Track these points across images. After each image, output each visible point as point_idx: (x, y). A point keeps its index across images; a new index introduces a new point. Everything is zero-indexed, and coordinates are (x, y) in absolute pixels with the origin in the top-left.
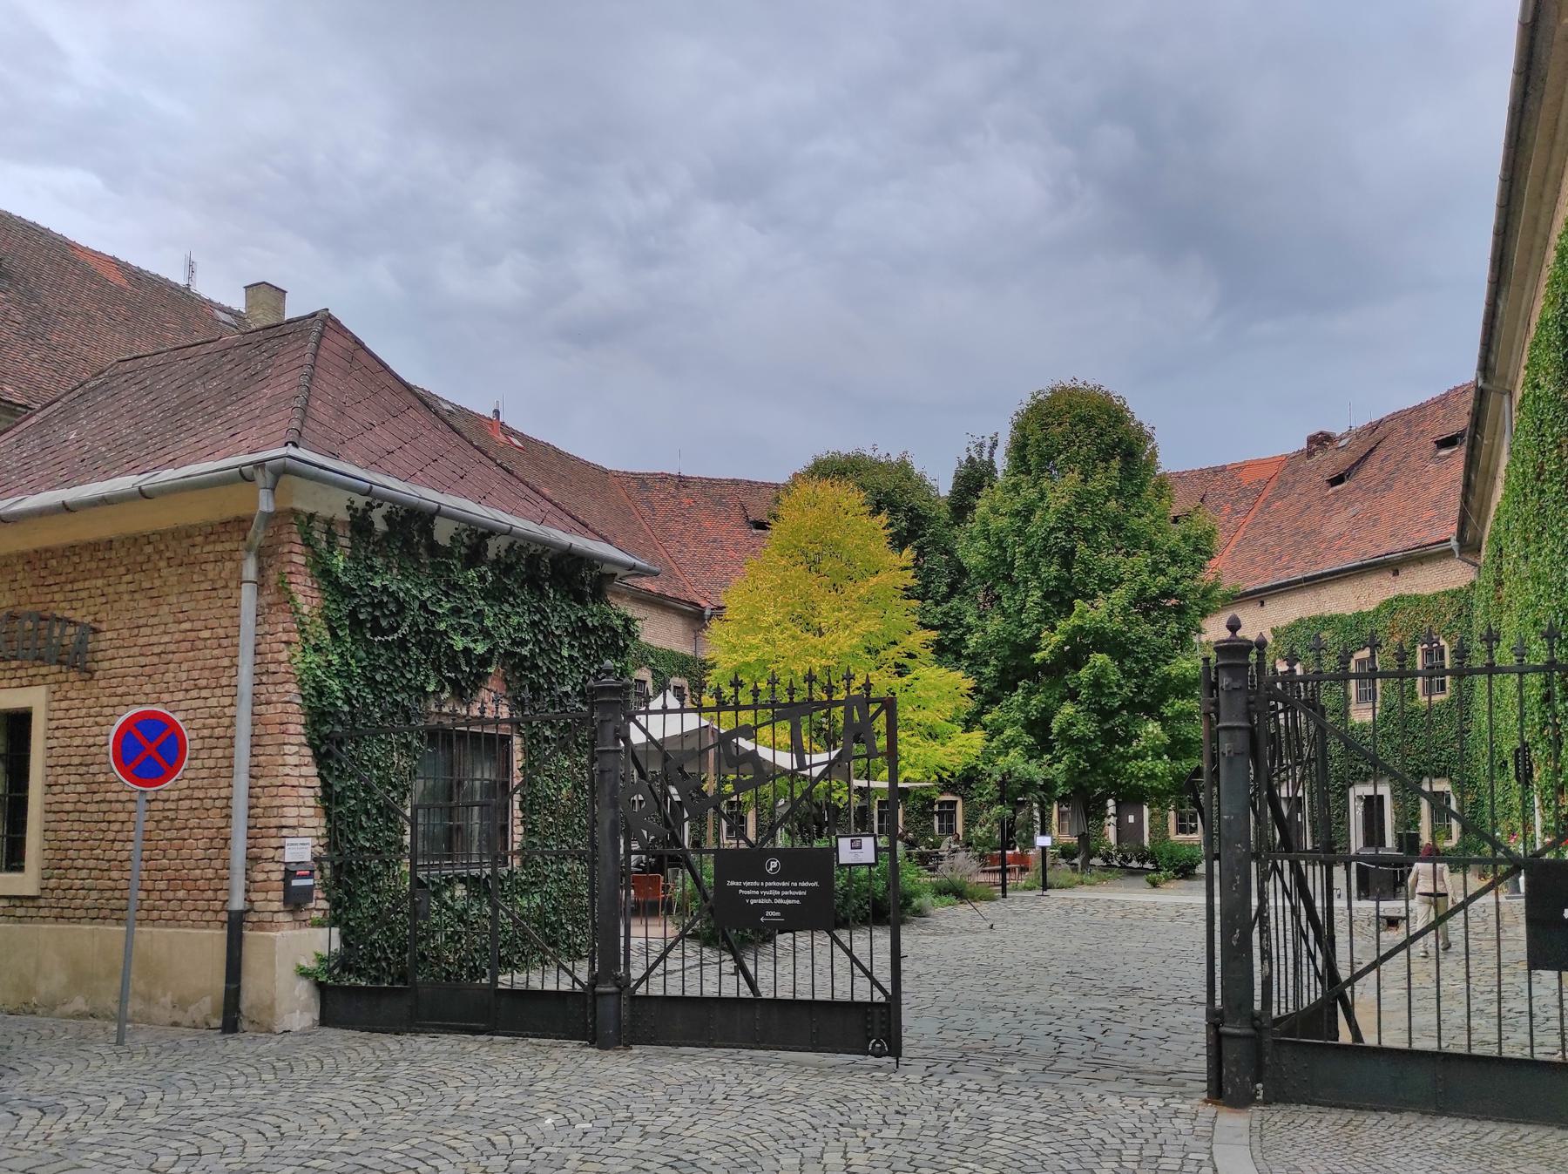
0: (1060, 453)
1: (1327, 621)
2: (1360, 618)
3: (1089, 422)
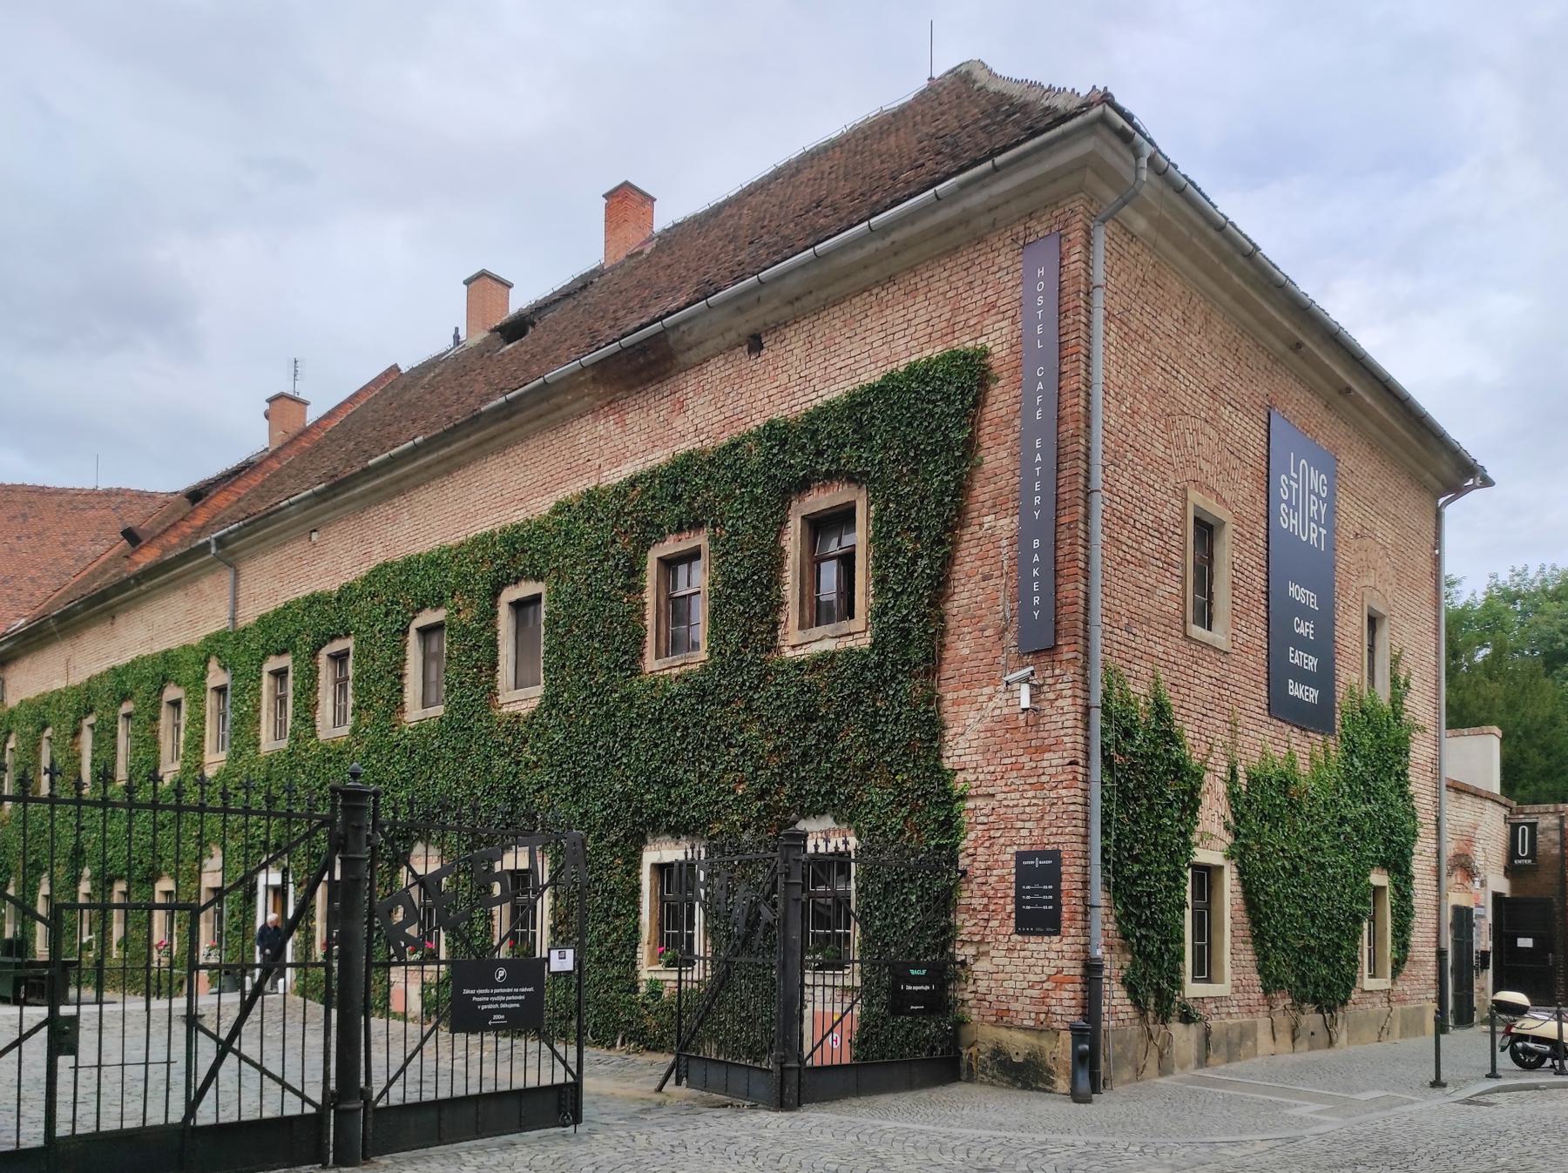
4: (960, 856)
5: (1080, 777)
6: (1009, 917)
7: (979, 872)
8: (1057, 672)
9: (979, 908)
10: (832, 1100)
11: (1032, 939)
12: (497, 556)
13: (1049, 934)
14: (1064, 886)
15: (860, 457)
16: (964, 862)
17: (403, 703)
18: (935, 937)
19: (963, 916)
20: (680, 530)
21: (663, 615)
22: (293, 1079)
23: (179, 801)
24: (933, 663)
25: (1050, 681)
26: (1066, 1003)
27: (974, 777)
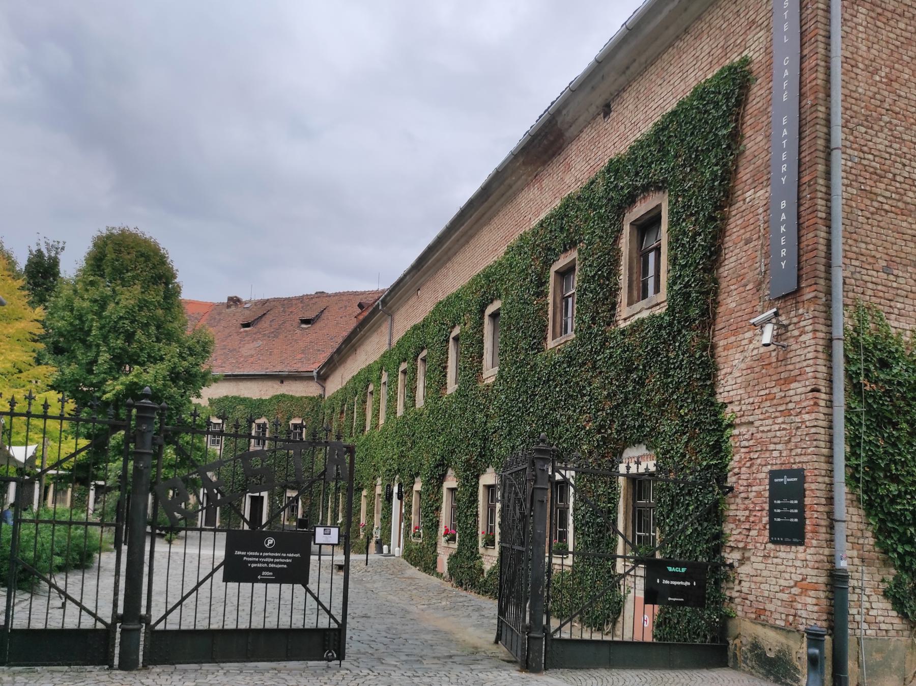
0: (128, 271)
1: (243, 401)
2: (261, 402)
3: (147, 258)
4: (730, 474)
5: (822, 403)
6: (765, 527)
7: (742, 488)
8: (801, 311)
9: (743, 519)
10: (581, 668)
11: (782, 548)
12: (482, 287)
13: (796, 544)
14: (808, 501)
15: (661, 169)
16: (731, 480)
17: (446, 383)
18: (707, 542)
19: (732, 526)
20: (565, 250)
21: (558, 310)
22: (89, 604)
23: (12, 409)
24: (708, 317)
25: (795, 320)
26: (810, 608)
27: (738, 408)
